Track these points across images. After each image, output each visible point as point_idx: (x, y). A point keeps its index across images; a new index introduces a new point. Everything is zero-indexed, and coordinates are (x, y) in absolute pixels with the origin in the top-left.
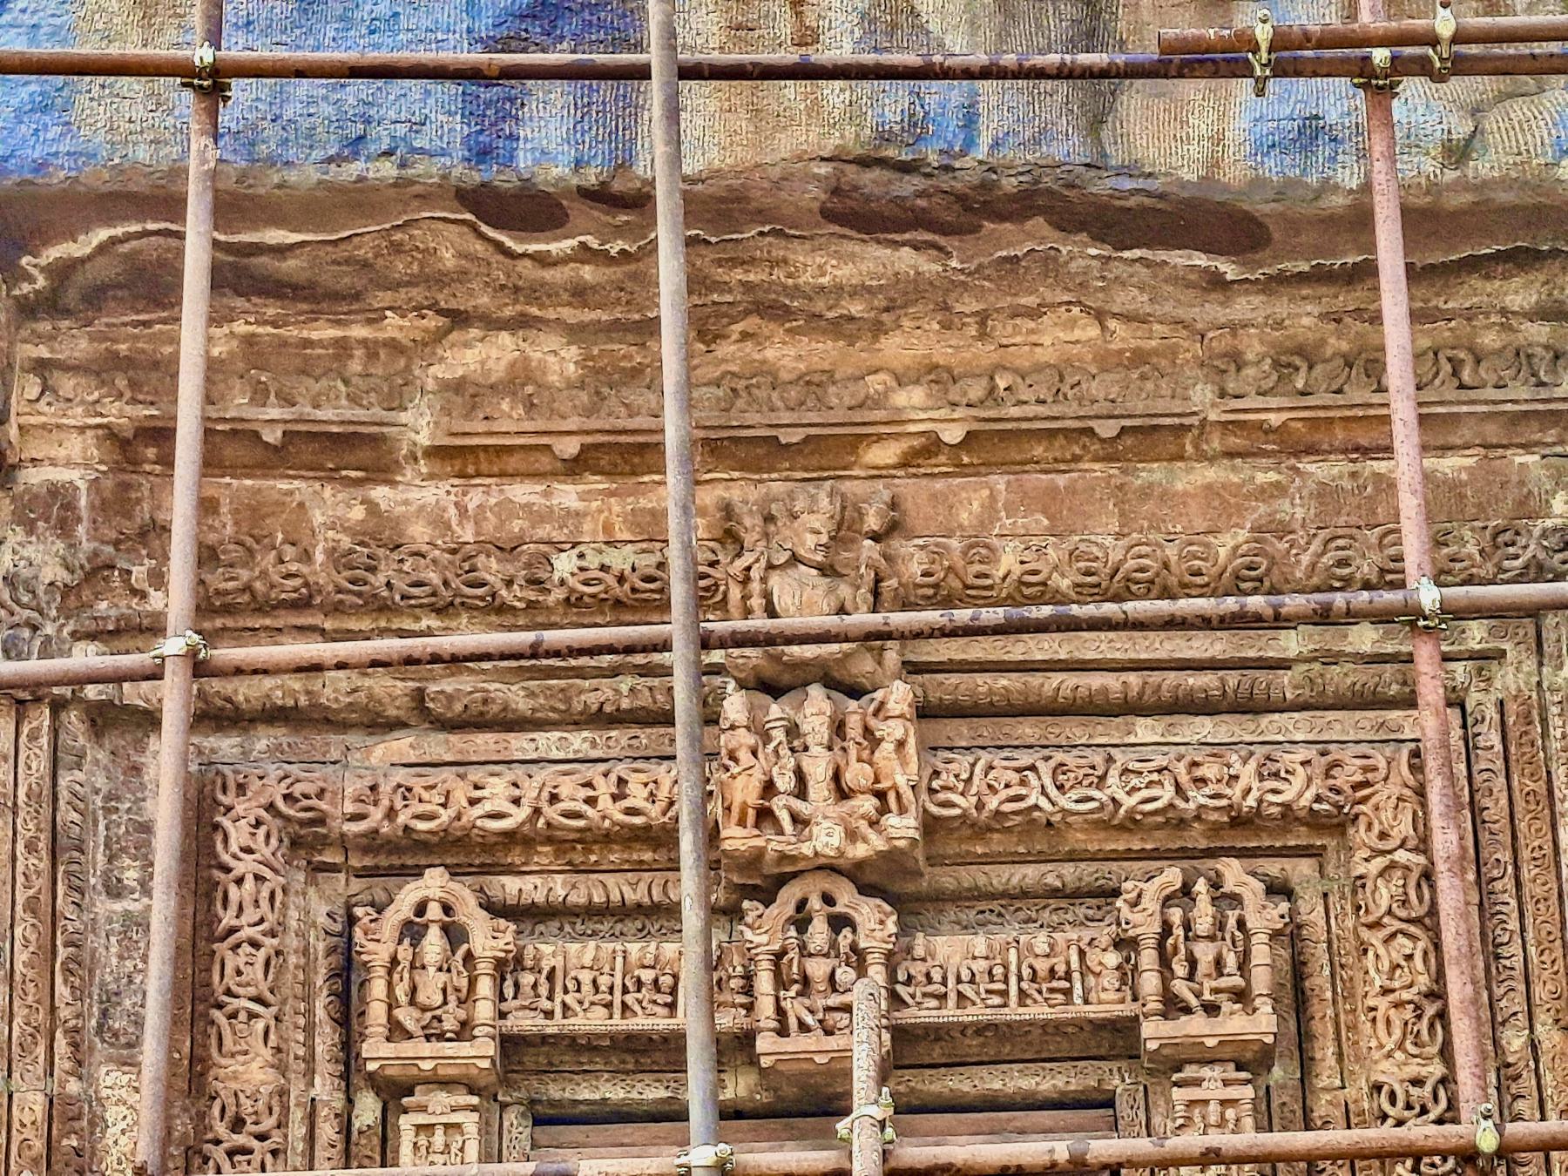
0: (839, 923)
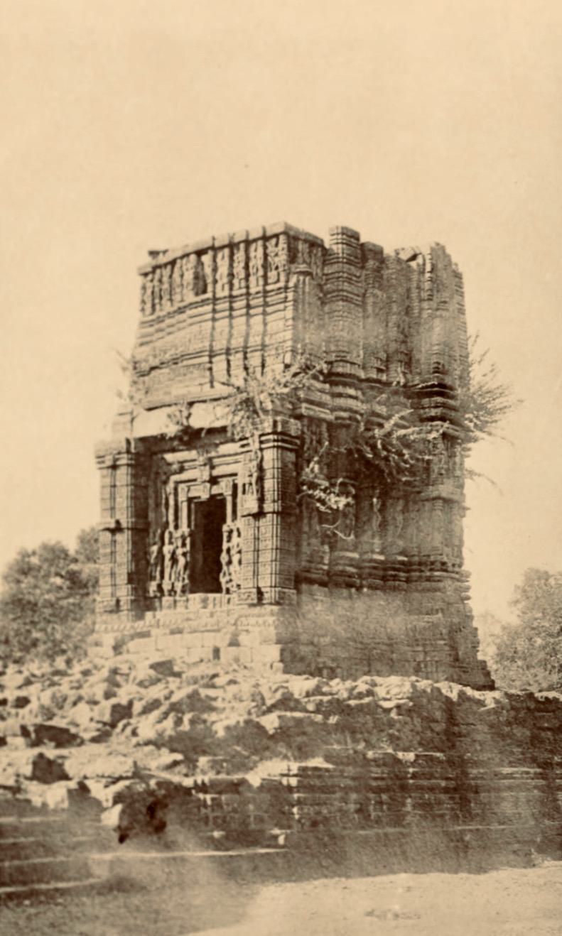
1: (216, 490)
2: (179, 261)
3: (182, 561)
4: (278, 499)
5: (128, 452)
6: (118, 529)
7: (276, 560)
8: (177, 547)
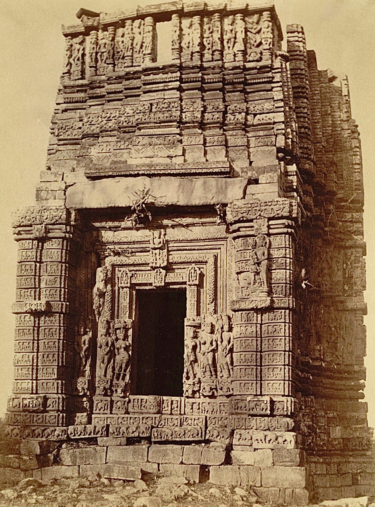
0: (160, 272)
1: (172, 278)
2: (129, 22)
3: (122, 357)
4: (290, 294)
5: (67, 223)
6: (48, 312)
7: (288, 365)
8: (117, 339)
